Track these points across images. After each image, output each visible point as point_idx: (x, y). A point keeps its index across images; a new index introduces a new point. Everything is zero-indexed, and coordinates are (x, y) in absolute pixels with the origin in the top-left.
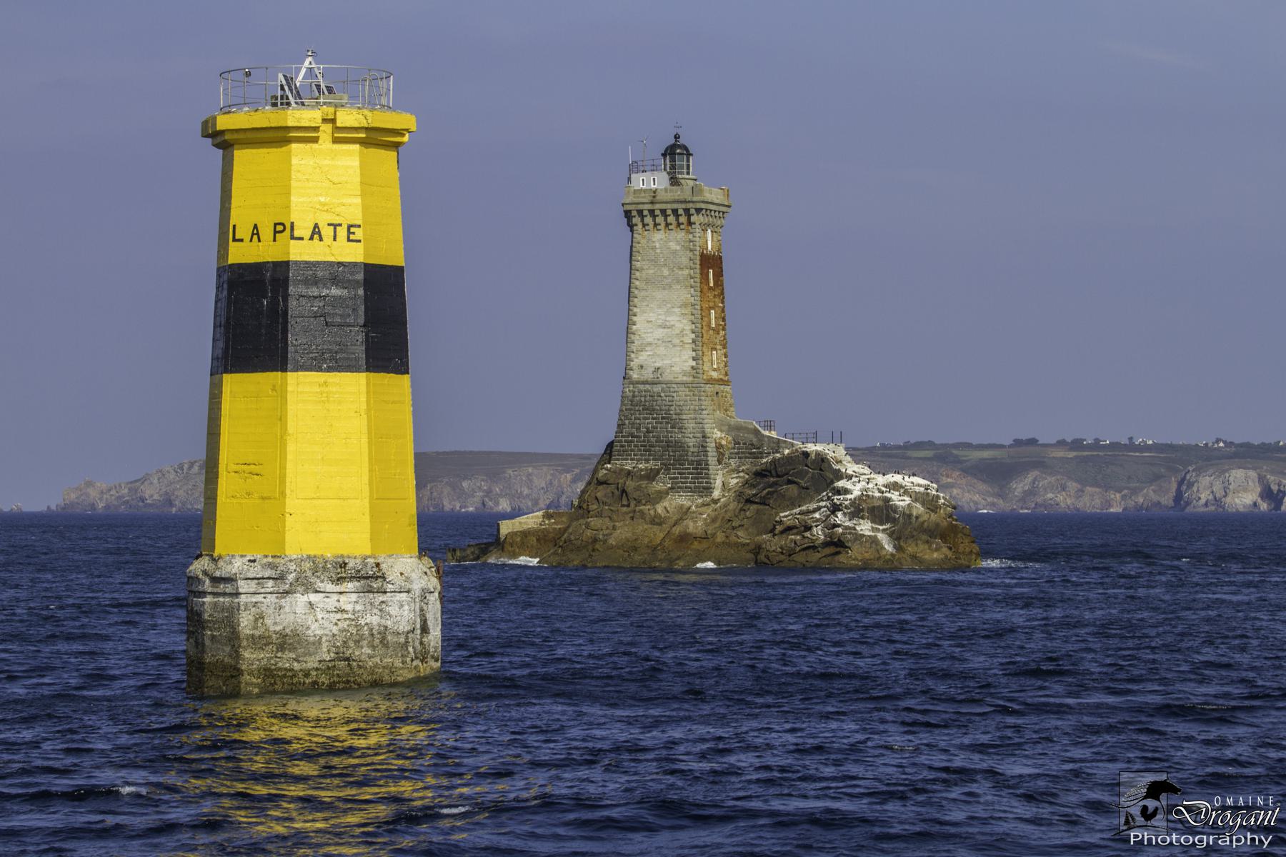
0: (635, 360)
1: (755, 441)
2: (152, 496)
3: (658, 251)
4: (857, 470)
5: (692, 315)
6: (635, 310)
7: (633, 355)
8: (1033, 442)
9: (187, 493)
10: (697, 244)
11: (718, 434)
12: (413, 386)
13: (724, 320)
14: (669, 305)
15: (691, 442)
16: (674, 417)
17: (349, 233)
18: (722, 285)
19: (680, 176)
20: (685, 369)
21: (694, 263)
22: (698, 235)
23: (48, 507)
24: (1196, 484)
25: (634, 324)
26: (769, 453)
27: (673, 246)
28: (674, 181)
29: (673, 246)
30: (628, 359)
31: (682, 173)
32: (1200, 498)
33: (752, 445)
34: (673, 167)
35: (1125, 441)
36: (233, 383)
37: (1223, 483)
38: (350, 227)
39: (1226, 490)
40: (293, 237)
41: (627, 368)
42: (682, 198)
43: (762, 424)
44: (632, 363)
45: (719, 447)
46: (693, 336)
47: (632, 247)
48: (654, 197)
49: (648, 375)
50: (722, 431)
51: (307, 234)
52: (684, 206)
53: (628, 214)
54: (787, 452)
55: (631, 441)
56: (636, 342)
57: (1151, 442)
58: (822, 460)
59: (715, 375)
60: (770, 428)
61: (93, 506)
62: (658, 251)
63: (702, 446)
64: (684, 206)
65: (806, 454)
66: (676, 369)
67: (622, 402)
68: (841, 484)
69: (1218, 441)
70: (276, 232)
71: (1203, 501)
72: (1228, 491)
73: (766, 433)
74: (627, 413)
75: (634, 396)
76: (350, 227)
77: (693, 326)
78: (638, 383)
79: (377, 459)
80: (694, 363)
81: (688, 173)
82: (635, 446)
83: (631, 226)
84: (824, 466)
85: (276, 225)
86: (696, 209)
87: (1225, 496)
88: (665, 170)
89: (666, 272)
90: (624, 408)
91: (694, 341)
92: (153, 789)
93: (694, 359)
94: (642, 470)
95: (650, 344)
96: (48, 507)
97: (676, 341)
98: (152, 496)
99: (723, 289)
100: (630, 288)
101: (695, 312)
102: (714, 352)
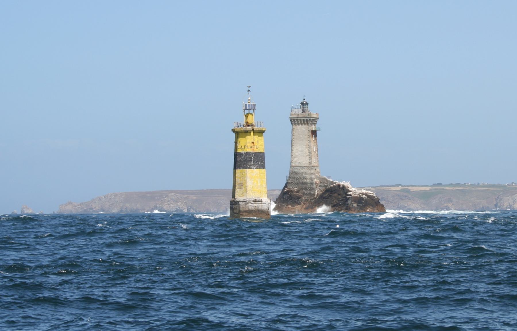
0: (293, 160)
1: (326, 182)
2: (95, 207)
3: (299, 130)
4: (353, 189)
5: (309, 148)
6: (293, 146)
7: (293, 159)
8: (440, 184)
9: (110, 206)
10: (310, 129)
11: (316, 180)
12: (266, 171)
13: (317, 149)
14: (302, 145)
15: (308, 182)
16: (304, 175)
17: (256, 147)
18: (317, 140)
19: (305, 110)
20: (307, 162)
21: (309, 134)
22: (310, 126)
23: (54, 212)
24: (502, 200)
25: (293, 150)
26: (329, 185)
27: (304, 129)
28: (303, 111)
29: (304, 129)
30: (291, 160)
31: (306, 109)
32: (504, 205)
33: (325, 183)
34: (303, 108)
35: (476, 184)
36: (238, 171)
37: (513, 199)
38: (256, 146)
39: (514, 201)
40: (247, 148)
41: (291, 163)
42: (306, 116)
43: (328, 177)
44: (292, 161)
45: (316, 184)
46: (309, 154)
47: (292, 129)
48: (298, 116)
49: (297, 164)
50: (316, 179)
51: (250, 147)
52: (306, 118)
53: (291, 120)
54: (334, 185)
55: (292, 182)
56: (293, 155)
57: (486, 184)
58: (344, 187)
59: (315, 164)
60: (330, 178)
61: (72, 211)
62: (299, 130)
63: (312, 183)
64: (306, 118)
65: (339, 185)
66: (304, 162)
67: (290, 171)
68: (349, 193)
69: (512, 183)
70: (245, 147)
71: (505, 206)
72: (515, 202)
73: (329, 180)
74: (291, 174)
75: (293, 170)
76: (256, 146)
77: (309, 151)
78: (294, 166)
79: (144, 196)
80: (309, 161)
81: (307, 109)
82: (293, 183)
83: (292, 124)
84: (344, 189)
85: (245, 146)
86: (310, 119)
87: (514, 204)
88: (301, 108)
89: (301, 136)
90: (290, 173)
91: (309, 155)
92: (209, 248)
93: (309, 160)
94: (295, 190)
95: (297, 156)
96: (54, 212)
97: (304, 155)
98: (95, 207)
99: (317, 141)
100: (292, 141)
101: (309, 147)
102: (315, 158)
